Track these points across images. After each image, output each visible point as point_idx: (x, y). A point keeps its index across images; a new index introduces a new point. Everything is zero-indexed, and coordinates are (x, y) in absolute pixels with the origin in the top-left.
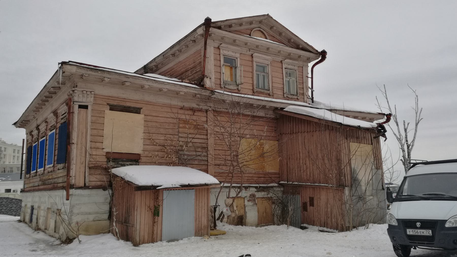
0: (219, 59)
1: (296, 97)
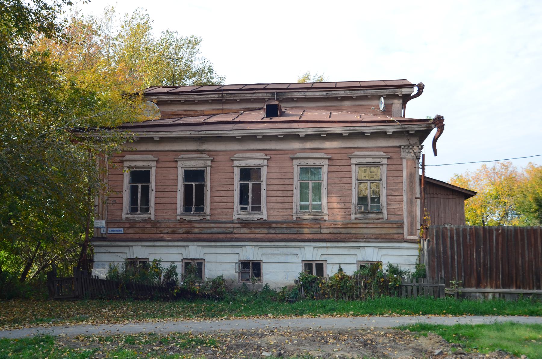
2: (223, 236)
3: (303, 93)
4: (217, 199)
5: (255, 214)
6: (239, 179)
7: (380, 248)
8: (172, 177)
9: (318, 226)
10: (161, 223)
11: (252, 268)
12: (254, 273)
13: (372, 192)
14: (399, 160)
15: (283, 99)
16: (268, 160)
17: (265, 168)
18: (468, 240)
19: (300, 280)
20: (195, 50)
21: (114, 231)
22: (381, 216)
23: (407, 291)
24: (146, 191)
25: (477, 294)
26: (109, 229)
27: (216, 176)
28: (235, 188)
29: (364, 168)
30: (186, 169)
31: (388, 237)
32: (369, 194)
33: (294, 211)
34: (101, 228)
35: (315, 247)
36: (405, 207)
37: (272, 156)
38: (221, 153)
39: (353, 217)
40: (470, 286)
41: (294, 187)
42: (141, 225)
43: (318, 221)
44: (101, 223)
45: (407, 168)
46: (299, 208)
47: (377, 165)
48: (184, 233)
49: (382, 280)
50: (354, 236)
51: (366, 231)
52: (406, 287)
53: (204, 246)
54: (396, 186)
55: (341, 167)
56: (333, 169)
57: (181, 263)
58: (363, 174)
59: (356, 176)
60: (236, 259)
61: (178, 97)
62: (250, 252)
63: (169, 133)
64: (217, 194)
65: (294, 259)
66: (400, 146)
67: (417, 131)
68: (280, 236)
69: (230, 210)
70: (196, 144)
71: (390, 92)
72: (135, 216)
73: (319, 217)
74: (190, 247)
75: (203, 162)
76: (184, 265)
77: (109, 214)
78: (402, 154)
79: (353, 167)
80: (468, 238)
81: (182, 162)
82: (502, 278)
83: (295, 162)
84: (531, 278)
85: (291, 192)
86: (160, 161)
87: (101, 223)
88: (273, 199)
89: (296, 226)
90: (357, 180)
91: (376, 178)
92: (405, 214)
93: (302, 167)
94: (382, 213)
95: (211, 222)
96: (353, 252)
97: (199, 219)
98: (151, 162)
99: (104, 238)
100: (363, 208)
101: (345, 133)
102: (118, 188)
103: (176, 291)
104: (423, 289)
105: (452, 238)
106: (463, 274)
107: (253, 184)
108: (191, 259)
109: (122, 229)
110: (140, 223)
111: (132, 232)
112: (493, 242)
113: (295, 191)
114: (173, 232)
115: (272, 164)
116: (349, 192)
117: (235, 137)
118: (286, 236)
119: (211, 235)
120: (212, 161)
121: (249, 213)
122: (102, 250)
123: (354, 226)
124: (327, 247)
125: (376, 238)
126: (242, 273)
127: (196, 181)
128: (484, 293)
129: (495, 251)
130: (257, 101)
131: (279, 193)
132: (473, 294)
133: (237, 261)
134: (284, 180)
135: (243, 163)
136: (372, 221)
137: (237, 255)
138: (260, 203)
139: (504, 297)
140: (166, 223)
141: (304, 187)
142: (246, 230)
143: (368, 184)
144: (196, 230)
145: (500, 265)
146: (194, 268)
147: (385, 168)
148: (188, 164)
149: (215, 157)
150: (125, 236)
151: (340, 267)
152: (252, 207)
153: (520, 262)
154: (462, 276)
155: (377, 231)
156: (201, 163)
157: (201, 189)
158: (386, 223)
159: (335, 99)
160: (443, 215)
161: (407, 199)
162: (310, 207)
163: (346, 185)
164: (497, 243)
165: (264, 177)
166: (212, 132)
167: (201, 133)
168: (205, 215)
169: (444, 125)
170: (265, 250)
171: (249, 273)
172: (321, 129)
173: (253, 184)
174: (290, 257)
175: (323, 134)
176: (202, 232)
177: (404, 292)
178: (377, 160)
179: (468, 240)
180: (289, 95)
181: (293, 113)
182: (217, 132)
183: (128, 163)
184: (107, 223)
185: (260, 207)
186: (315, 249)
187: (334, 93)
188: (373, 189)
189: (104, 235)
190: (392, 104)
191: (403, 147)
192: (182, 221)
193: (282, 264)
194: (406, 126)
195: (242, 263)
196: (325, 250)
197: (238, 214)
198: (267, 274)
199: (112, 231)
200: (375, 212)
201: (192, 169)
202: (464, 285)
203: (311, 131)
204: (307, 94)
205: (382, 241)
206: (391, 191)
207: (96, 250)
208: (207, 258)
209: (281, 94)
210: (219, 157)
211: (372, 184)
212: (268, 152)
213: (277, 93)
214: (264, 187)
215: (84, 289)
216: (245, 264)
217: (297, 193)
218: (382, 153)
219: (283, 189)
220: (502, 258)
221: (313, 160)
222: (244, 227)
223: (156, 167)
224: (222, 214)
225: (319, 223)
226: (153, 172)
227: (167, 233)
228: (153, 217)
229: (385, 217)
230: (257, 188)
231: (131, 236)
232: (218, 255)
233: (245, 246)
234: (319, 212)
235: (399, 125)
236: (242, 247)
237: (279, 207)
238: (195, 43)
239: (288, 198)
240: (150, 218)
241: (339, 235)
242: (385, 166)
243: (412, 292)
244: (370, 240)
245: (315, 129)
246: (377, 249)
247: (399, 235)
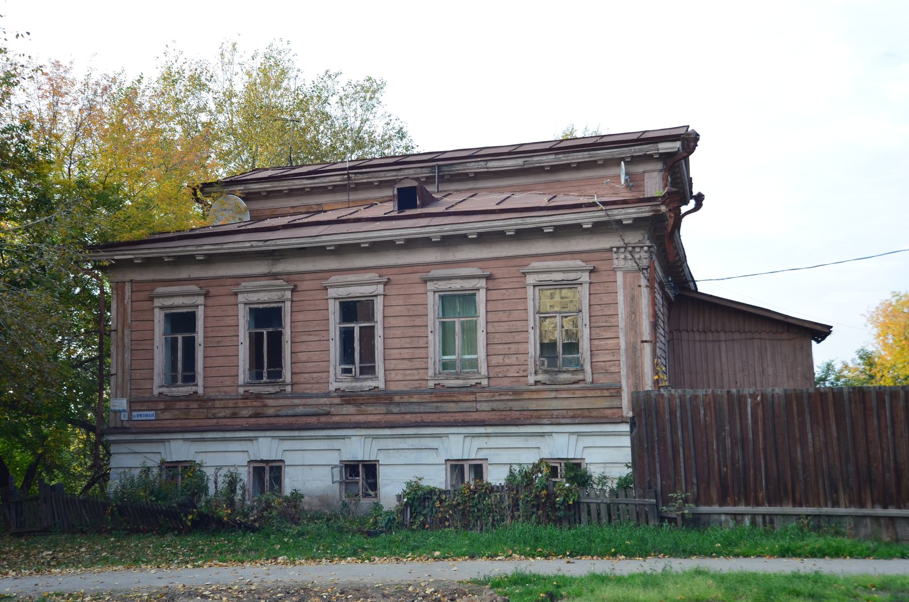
2: (313, 420)
3: (482, 163)
4: (302, 357)
5: (366, 379)
6: (338, 320)
7: (579, 434)
8: (230, 321)
9: (471, 398)
10: (214, 400)
11: (361, 474)
12: (368, 483)
13: (564, 333)
14: (611, 273)
15: (452, 176)
16: (385, 284)
17: (380, 299)
18: (702, 416)
19: (405, 494)
20: (374, 101)
21: (141, 415)
22: (580, 377)
23: (589, 514)
24: (190, 345)
25: (723, 518)
26: (134, 413)
27: (300, 317)
28: (332, 335)
29: (548, 292)
30: (252, 306)
31: (594, 413)
32: (559, 337)
33: (431, 372)
34: (120, 411)
35: (466, 436)
36: (623, 359)
37: (391, 277)
38: (308, 276)
39: (531, 379)
40: (709, 503)
41: (430, 330)
42: (183, 405)
43: (471, 389)
44: (121, 404)
45: (625, 288)
46: (439, 367)
47: (573, 285)
48: (250, 417)
49: (544, 492)
50: (535, 413)
51: (555, 404)
52: (588, 504)
54: (606, 321)
56: (494, 295)
57: (246, 469)
58: (549, 302)
59: (534, 307)
60: (334, 459)
61: (276, 184)
62: (357, 447)
63: (217, 247)
64: (302, 347)
65: (431, 457)
66: (610, 250)
67: (635, 219)
68: (408, 417)
69: (324, 375)
70: (266, 262)
71: (638, 150)
72: (174, 389)
73: (473, 382)
74: (260, 440)
75: (279, 293)
76: (251, 471)
77: (133, 387)
78: (615, 261)
79: (530, 290)
80: (702, 412)
81: (246, 295)
82: (767, 486)
83: (431, 286)
84: (821, 486)
85: (425, 339)
86: (299, 289)
87: (121, 404)
88: (395, 353)
89: (435, 399)
90: (539, 312)
91: (571, 307)
92: (624, 372)
93: (442, 293)
94: (583, 370)
95: (294, 395)
96: (533, 442)
97: (274, 391)
98: (196, 298)
99: (126, 428)
100: (546, 363)
101: (509, 231)
102: (143, 345)
103: (190, 517)
104: (618, 509)
105: (672, 413)
106: (695, 481)
107: (360, 328)
108: (262, 461)
109: (153, 412)
110: (181, 400)
111: (168, 417)
112: (747, 419)
113: (431, 336)
114: (234, 416)
115: (392, 290)
116: (524, 335)
117: (324, 247)
118: (418, 418)
119: (294, 419)
120: (293, 291)
121: (355, 379)
122: (123, 448)
123: (535, 396)
124: (488, 435)
125: (573, 417)
126: (346, 483)
127: (269, 327)
128: (735, 514)
129: (751, 436)
130: (382, 185)
131: (405, 342)
132: (716, 517)
133: (338, 463)
134: (413, 318)
135: (343, 292)
136: (566, 386)
137: (337, 453)
138: (373, 361)
139: (772, 522)
140: (222, 399)
141: (446, 330)
142: (351, 409)
143: (558, 320)
144: (271, 411)
145: (763, 462)
146: (268, 473)
147: (585, 290)
148: (254, 297)
149: (299, 284)
150: (158, 425)
151: (511, 471)
152: (361, 368)
153: (799, 455)
154: (693, 483)
155: (574, 404)
156: (274, 296)
157: (276, 340)
158: (589, 389)
159: (539, 170)
160: (770, 371)
161: (626, 344)
162: (458, 364)
163: (519, 323)
164: (755, 421)
165: (378, 316)
166: (285, 242)
167: (268, 243)
168: (284, 384)
170: (383, 443)
171: (357, 483)
172: (466, 226)
173: (360, 328)
174: (425, 454)
175: (471, 234)
176: (281, 413)
177: (584, 516)
178: (572, 276)
179: (702, 416)
180: (460, 169)
181: (454, 198)
182: (293, 241)
183: (161, 300)
184: (130, 403)
185: (374, 367)
186: (468, 440)
187: (537, 161)
188: (566, 328)
189: (125, 424)
190: (644, 172)
191: (615, 250)
192: (247, 397)
193: (412, 467)
194: (616, 212)
195: (346, 466)
196: (485, 439)
197: (337, 380)
198: (387, 485)
199: (138, 416)
200: (571, 369)
201: (261, 306)
202: (697, 502)
203: (448, 230)
204: (490, 164)
205: (587, 421)
206: (598, 330)
207: (113, 449)
208: (289, 459)
209: (446, 169)
210: (305, 283)
211: (565, 319)
212: (384, 271)
213: (439, 166)
214: (379, 331)
215: (56, 516)
216: (350, 467)
217: (434, 340)
218: (579, 263)
219: (411, 334)
220: (765, 449)
222: (348, 403)
223: (205, 306)
224: (311, 381)
225: (474, 393)
226: (200, 313)
227: (225, 417)
228: (200, 390)
229: (589, 378)
230: (368, 334)
231: (167, 424)
232: (306, 452)
233: (349, 437)
234: (474, 373)
235: (602, 210)
236: (344, 437)
237: (404, 367)
238: (369, 92)
239: (420, 350)
240: (196, 393)
241: (508, 413)
242: (586, 286)
243: (599, 514)
244: (562, 421)
245: (455, 227)
246: (575, 437)
247: (615, 411)
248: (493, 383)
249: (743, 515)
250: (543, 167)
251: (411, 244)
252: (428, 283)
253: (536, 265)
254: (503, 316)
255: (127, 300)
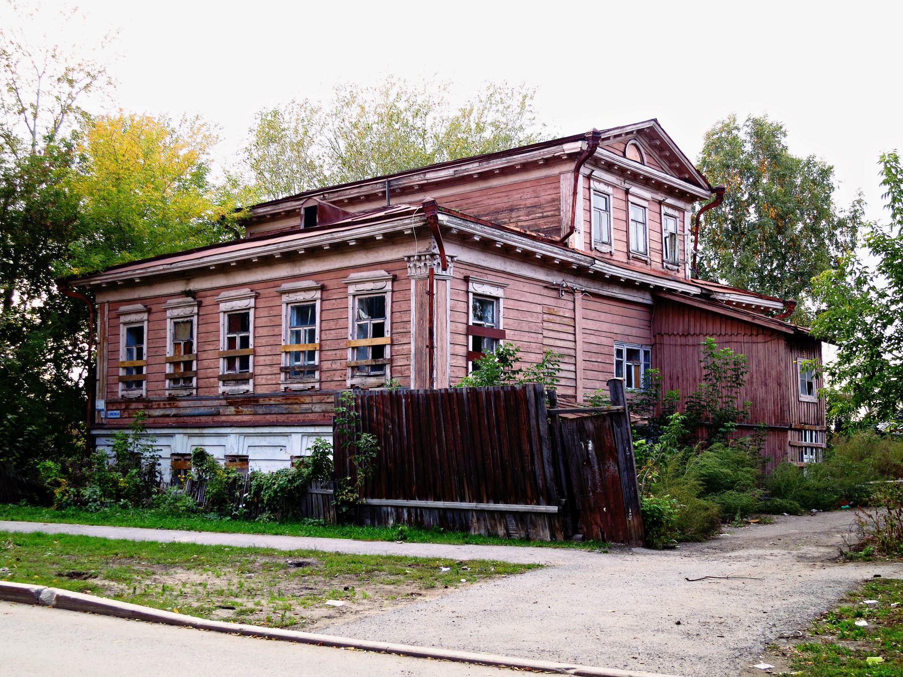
0: (587, 197)
1: (676, 268)
6: (226, 331)
16: (256, 298)
26: (109, 412)
27: (203, 328)
35: (304, 435)
36: (413, 362)
38: (209, 293)
45: (416, 296)
53: (247, 435)
54: (404, 328)
55: (338, 301)
83: (285, 298)
92: (413, 376)
95: (199, 398)
99: (103, 424)
142: (232, 409)
168: (192, 388)
169: (832, 188)
173: (241, 337)
180: (405, 182)
184: (107, 403)
186: (305, 438)
190: (560, 174)
207: (98, 441)
209: (394, 183)
210: (208, 299)
213: (389, 182)
221: (303, 293)
222: (231, 404)
245: (287, 244)
248: (324, 386)
249: (403, 507)
250: (471, 175)
251: (267, 261)
252: (283, 296)
253: (354, 276)
254: (332, 325)
255: (106, 319)
